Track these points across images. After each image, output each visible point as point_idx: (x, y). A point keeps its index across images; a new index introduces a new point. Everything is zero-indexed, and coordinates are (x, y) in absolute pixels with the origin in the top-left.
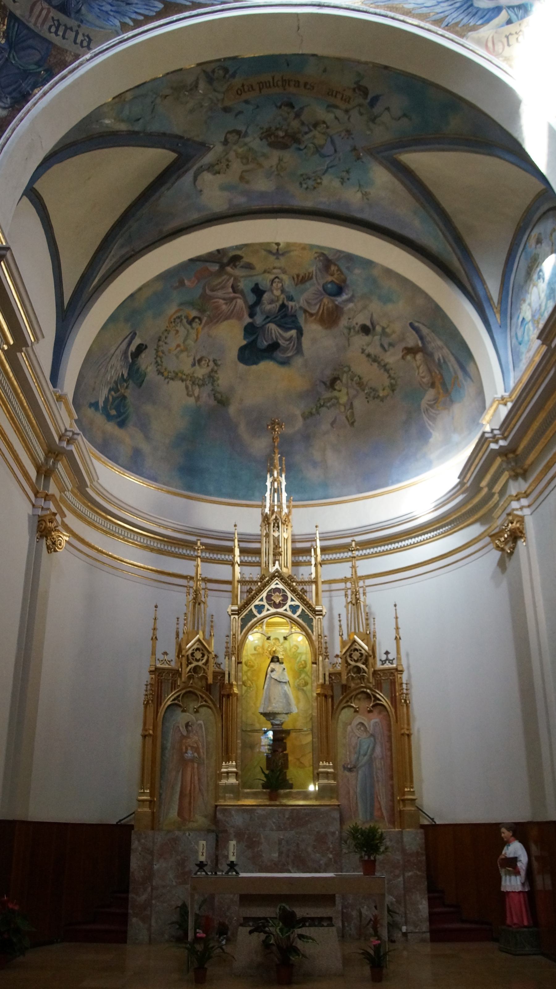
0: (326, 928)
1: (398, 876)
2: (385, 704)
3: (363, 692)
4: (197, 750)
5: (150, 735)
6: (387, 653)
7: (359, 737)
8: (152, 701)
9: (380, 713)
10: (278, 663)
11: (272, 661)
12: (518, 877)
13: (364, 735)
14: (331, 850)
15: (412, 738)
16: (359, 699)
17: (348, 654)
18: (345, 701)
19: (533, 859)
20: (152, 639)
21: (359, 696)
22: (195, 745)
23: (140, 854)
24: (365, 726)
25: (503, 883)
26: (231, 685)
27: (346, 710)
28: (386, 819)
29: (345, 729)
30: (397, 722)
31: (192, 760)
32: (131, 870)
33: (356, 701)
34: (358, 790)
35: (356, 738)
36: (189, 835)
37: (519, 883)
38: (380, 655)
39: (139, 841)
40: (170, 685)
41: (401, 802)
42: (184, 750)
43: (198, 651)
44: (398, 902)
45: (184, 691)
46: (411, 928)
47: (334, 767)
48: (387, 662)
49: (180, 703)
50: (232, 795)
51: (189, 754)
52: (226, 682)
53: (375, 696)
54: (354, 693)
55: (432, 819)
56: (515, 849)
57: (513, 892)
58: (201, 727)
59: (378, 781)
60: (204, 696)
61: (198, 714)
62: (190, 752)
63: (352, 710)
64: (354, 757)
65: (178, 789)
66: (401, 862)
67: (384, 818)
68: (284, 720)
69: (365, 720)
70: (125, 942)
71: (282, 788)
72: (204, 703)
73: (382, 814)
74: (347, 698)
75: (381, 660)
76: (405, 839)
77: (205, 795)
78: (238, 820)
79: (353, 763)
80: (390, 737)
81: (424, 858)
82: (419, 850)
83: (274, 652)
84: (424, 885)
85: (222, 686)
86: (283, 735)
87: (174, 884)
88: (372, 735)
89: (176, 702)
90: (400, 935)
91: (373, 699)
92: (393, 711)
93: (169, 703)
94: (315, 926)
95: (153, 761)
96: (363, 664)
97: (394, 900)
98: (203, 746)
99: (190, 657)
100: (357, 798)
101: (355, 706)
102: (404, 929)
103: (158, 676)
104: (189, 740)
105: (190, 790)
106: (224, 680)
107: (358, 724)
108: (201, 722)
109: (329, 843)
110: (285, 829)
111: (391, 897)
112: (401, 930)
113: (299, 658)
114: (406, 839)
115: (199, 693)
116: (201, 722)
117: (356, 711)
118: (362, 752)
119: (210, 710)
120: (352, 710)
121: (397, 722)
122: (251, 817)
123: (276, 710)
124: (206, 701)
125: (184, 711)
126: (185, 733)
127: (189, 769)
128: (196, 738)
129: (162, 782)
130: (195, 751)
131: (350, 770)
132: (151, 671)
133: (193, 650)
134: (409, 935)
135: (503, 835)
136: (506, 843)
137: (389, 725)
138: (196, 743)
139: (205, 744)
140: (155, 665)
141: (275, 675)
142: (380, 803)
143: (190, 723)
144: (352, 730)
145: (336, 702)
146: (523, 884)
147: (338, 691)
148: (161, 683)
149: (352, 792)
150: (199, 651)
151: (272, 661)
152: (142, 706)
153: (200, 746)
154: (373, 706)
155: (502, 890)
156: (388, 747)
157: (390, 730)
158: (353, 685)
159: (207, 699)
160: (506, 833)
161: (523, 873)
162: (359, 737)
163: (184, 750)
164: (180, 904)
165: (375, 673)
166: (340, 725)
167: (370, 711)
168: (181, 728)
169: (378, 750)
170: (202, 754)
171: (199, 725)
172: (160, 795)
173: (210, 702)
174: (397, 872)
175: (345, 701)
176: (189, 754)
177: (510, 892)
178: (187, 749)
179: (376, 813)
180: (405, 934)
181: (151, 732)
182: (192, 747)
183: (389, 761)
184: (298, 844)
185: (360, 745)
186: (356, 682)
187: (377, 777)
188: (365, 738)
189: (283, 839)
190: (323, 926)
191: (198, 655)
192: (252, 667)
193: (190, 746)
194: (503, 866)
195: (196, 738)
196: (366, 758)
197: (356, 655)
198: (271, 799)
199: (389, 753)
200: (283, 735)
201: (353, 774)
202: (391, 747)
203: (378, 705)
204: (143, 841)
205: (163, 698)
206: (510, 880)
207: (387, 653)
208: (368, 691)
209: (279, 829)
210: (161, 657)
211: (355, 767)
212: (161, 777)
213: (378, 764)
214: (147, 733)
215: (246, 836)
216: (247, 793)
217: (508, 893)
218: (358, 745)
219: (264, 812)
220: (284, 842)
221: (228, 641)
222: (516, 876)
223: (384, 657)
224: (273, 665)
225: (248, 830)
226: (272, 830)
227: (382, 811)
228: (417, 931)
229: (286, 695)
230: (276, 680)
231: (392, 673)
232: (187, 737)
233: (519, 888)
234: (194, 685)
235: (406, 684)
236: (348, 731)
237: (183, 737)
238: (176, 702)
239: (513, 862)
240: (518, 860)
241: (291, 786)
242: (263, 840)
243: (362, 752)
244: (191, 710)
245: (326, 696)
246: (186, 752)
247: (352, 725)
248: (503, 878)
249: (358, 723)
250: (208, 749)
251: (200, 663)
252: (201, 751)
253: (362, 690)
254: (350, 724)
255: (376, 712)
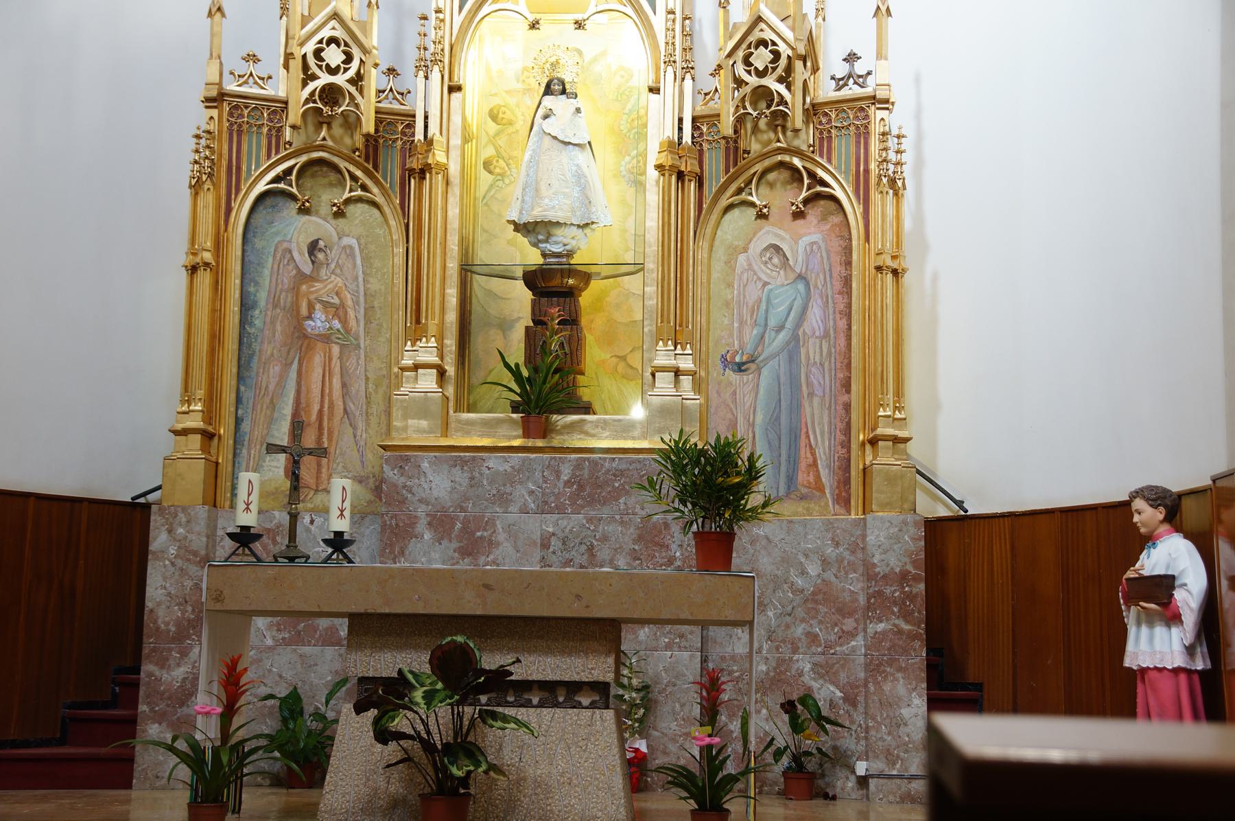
0: (588, 713)
1: (852, 635)
2: (839, 194)
3: (781, 164)
4: (338, 311)
5: (207, 264)
6: (851, 58)
7: (766, 284)
8: (210, 175)
9: (824, 218)
10: (564, 97)
11: (548, 91)
12: (1175, 631)
13: (781, 278)
14: (678, 563)
15: (907, 279)
16: (771, 185)
17: (740, 54)
18: (733, 188)
19: (1224, 584)
20: (210, 14)
21: (771, 176)
22: (336, 300)
23: (173, 564)
24: (785, 255)
25: (1130, 647)
26: (429, 142)
27: (736, 212)
28: (827, 491)
29: (730, 263)
30: (867, 239)
31: (326, 338)
32: (149, 604)
33: (764, 190)
34: (759, 418)
35: (760, 285)
36: (312, 522)
37: (1177, 647)
38: (832, 63)
39: (170, 531)
40: (264, 142)
41: (868, 447)
42: (304, 311)
43: (344, 57)
44: (850, 700)
45: (304, 158)
46: (879, 766)
47: (699, 358)
48: (851, 81)
49: (294, 190)
50: (424, 423)
51: (319, 322)
52: (419, 136)
53: (812, 175)
54: (759, 168)
55: (960, 504)
56: (1173, 555)
57: (1156, 668)
58: (351, 255)
59: (811, 395)
60: (359, 173)
61: (341, 221)
62: (319, 314)
63: (752, 212)
64: (751, 335)
65: (288, 411)
66: (862, 600)
67: (821, 489)
68: (574, 243)
69: (783, 239)
70: (128, 785)
71: (562, 411)
72: (359, 192)
73: (818, 477)
74: (740, 182)
75: (833, 78)
76: (871, 539)
77: (361, 425)
78: (438, 484)
79: (749, 348)
80: (847, 281)
81: (922, 586)
82: (909, 568)
83: (554, 65)
84: (918, 656)
85: (410, 148)
86: (571, 281)
87: (269, 642)
88: (800, 277)
89: (282, 186)
90: (851, 784)
91: (806, 181)
92: (859, 210)
93: (261, 187)
94: (556, 705)
95: (216, 338)
96: (780, 80)
97: (839, 694)
98: (356, 303)
99: (311, 61)
100: (754, 437)
101: (758, 203)
102: (861, 768)
103: (231, 114)
104: (318, 285)
105: (321, 412)
106: (413, 135)
107: (766, 249)
108: (352, 242)
109: (674, 547)
110: (560, 509)
111: (832, 688)
112: (853, 772)
113: (633, 101)
114: (876, 536)
115: (343, 164)
116: (353, 242)
117: (761, 216)
118: (772, 323)
119: (376, 211)
120: (752, 212)
121: (867, 239)
122: (472, 478)
123: (552, 216)
124: (364, 188)
125: (304, 211)
126: (307, 268)
127: (318, 359)
128: (339, 281)
129: (242, 388)
130: (336, 315)
131: (740, 368)
132: (207, 100)
133: (321, 42)
134: (873, 783)
135: (1136, 518)
136: (1146, 540)
137: (848, 250)
138: (337, 294)
139: (362, 299)
140: (220, 84)
141: (551, 126)
142: (813, 454)
143: (321, 244)
144: (750, 267)
145: (710, 189)
146: (1190, 650)
147: (714, 163)
148: (240, 133)
149: (740, 421)
150: (338, 45)
151: (548, 91)
152: (187, 192)
153: (350, 303)
154: (806, 202)
155: (1127, 663)
156: (842, 307)
157: (848, 263)
158: (755, 147)
159: (369, 182)
160: (1146, 515)
161: (1190, 618)
162: (766, 284)
163: (304, 311)
164: (283, 692)
165: (813, 111)
166: (720, 253)
167: (798, 215)
168: (296, 255)
169: (815, 314)
170: (352, 323)
171: (344, 247)
172: (238, 421)
173: (375, 190)
174: (849, 624)
175: (733, 188)
176: (319, 322)
177: (1148, 668)
178: (311, 308)
179: (802, 477)
180: (863, 781)
181: (208, 256)
182: (326, 305)
183: (842, 342)
184: (591, 549)
185: (768, 301)
186: (765, 137)
187: (809, 384)
188: (783, 285)
189: (554, 534)
190: (578, 705)
191: (334, 56)
192: (511, 123)
193: (321, 302)
194: (1131, 600)
195: (339, 281)
196: (783, 336)
197: (761, 58)
198: (527, 434)
199: (842, 324)
200: (571, 281)
201: (748, 378)
202: (849, 305)
203: (821, 197)
204: (181, 530)
205: (244, 175)
206: (1151, 639)
207: (851, 58)
208: (797, 162)
209: (544, 508)
210: (243, 68)
211: (752, 360)
212: (240, 378)
213: (812, 350)
214: (198, 260)
215: (459, 525)
216: (470, 423)
217: (1144, 671)
218: (763, 306)
219: (507, 467)
220: (555, 543)
221: (422, 30)
222: (1169, 626)
223: (841, 70)
224: (549, 101)
225: (463, 510)
226: (524, 510)
227: (818, 471)
228: (895, 773)
229: (580, 177)
230: (555, 138)
231: (862, 109)
232: (312, 278)
233: (1177, 659)
234: (330, 143)
235: (898, 137)
236: (738, 270)
237: (302, 277)
238: (282, 186)
239: (1161, 589)
240: (1177, 583)
241: (587, 409)
242: (501, 537)
243: (772, 323)
244: (325, 209)
245: (681, 176)
246: (310, 317)
247: (751, 251)
248: (1132, 631)
249: (765, 245)
250: (369, 310)
251: (340, 80)
252: (351, 314)
253: (779, 158)
254: (745, 250)
255: (813, 213)
